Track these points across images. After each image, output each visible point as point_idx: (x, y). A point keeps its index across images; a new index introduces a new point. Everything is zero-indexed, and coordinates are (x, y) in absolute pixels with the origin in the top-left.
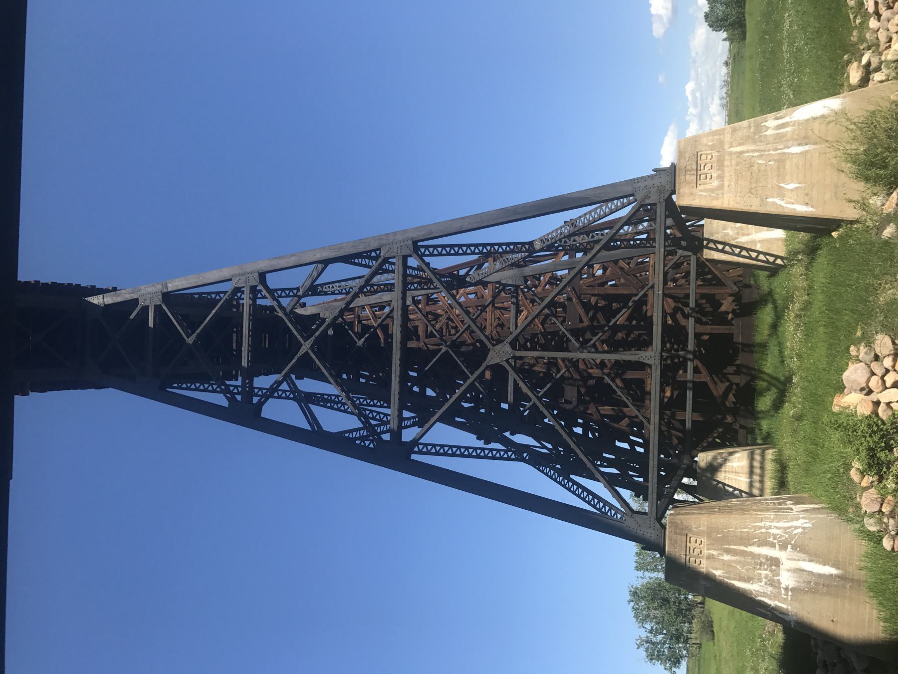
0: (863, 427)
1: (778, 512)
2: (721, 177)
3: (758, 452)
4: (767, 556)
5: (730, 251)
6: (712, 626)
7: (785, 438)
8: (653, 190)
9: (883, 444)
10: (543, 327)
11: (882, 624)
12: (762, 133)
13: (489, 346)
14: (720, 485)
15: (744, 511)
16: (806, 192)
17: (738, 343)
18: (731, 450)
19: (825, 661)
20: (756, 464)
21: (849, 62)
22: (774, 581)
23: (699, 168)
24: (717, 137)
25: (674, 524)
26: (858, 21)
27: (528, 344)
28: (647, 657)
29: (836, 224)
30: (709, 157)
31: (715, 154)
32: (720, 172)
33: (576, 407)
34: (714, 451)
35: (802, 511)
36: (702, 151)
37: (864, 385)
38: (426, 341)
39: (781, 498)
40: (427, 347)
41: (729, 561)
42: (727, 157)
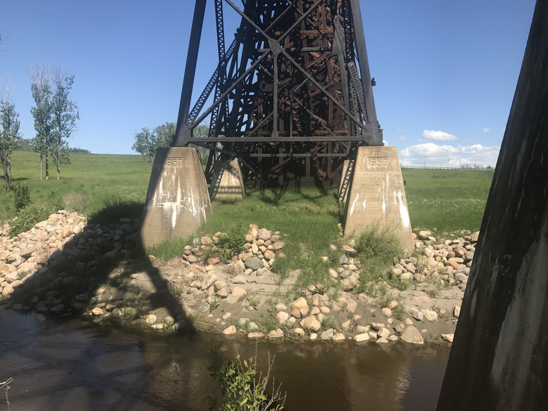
0: (239, 237)
1: (199, 201)
2: (372, 170)
3: (240, 190)
4: (177, 196)
5: (348, 174)
7: (248, 203)
8: (369, 134)
9: (231, 245)
10: (308, 68)
11: (152, 246)
12: (395, 190)
13: (280, 39)
14: (221, 172)
16: (361, 211)
17: (300, 179)
18: (241, 177)
19: (134, 223)
20: (234, 190)
21: (432, 230)
22: (165, 199)
23: (379, 158)
24: (395, 167)
25: (187, 151)
26: (452, 235)
27: (301, 58)
28: (139, 134)
29: (344, 226)
30: (385, 164)
31: (386, 166)
32: (375, 169)
33: (261, 91)
34: (239, 169)
35: (201, 212)
36: (388, 159)
37: (260, 237)
41: (172, 178)
42: (383, 173)
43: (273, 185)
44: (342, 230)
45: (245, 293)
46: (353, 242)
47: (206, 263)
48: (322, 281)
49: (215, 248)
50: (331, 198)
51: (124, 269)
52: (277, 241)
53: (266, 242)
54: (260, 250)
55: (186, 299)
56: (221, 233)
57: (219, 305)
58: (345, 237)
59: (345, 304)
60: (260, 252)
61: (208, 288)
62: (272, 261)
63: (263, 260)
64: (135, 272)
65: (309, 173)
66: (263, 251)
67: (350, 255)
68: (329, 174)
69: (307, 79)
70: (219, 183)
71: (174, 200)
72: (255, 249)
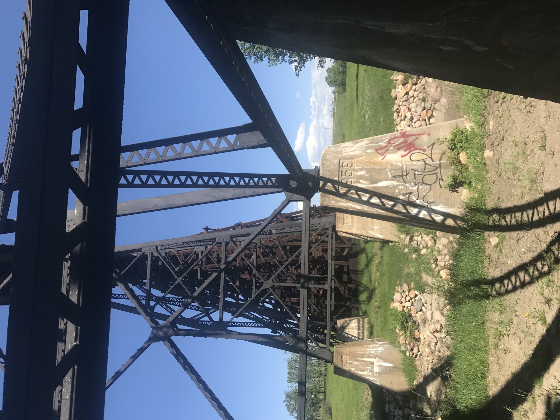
0: (400, 315)
2: (352, 222)
6: (331, 410)
11: (407, 382)
15: (362, 345)
20: (361, 325)
22: (372, 370)
25: (336, 351)
29: (391, 242)
38: (206, 266)
39: (373, 340)
40: (206, 269)
41: (357, 364)
43: (355, 293)
44: (394, 243)
45: (438, 311)
46: (403, 236)
47: (418, 340)
48: (429, 260)
49: (408, 334)
50: (368, 246)
51: (424, 403)
52: (402, 288)
53: (403, 296)
54: (409, 301)
55: (444, 354)
56: (397, 329)
57: (447, 330)
58: (399, 241)
59: (443, 246)
60: (411, 300)
61: (435, 337)
62: (417, 293)
63: (416, 298)
64: (427, 394)
65: (346, 262)
66: (410, 298)
67: (411, 239)
68: (347, 246)
69: (208, 254)
70: (355, 337)
71: (372, 363)
72: (408, 304)
